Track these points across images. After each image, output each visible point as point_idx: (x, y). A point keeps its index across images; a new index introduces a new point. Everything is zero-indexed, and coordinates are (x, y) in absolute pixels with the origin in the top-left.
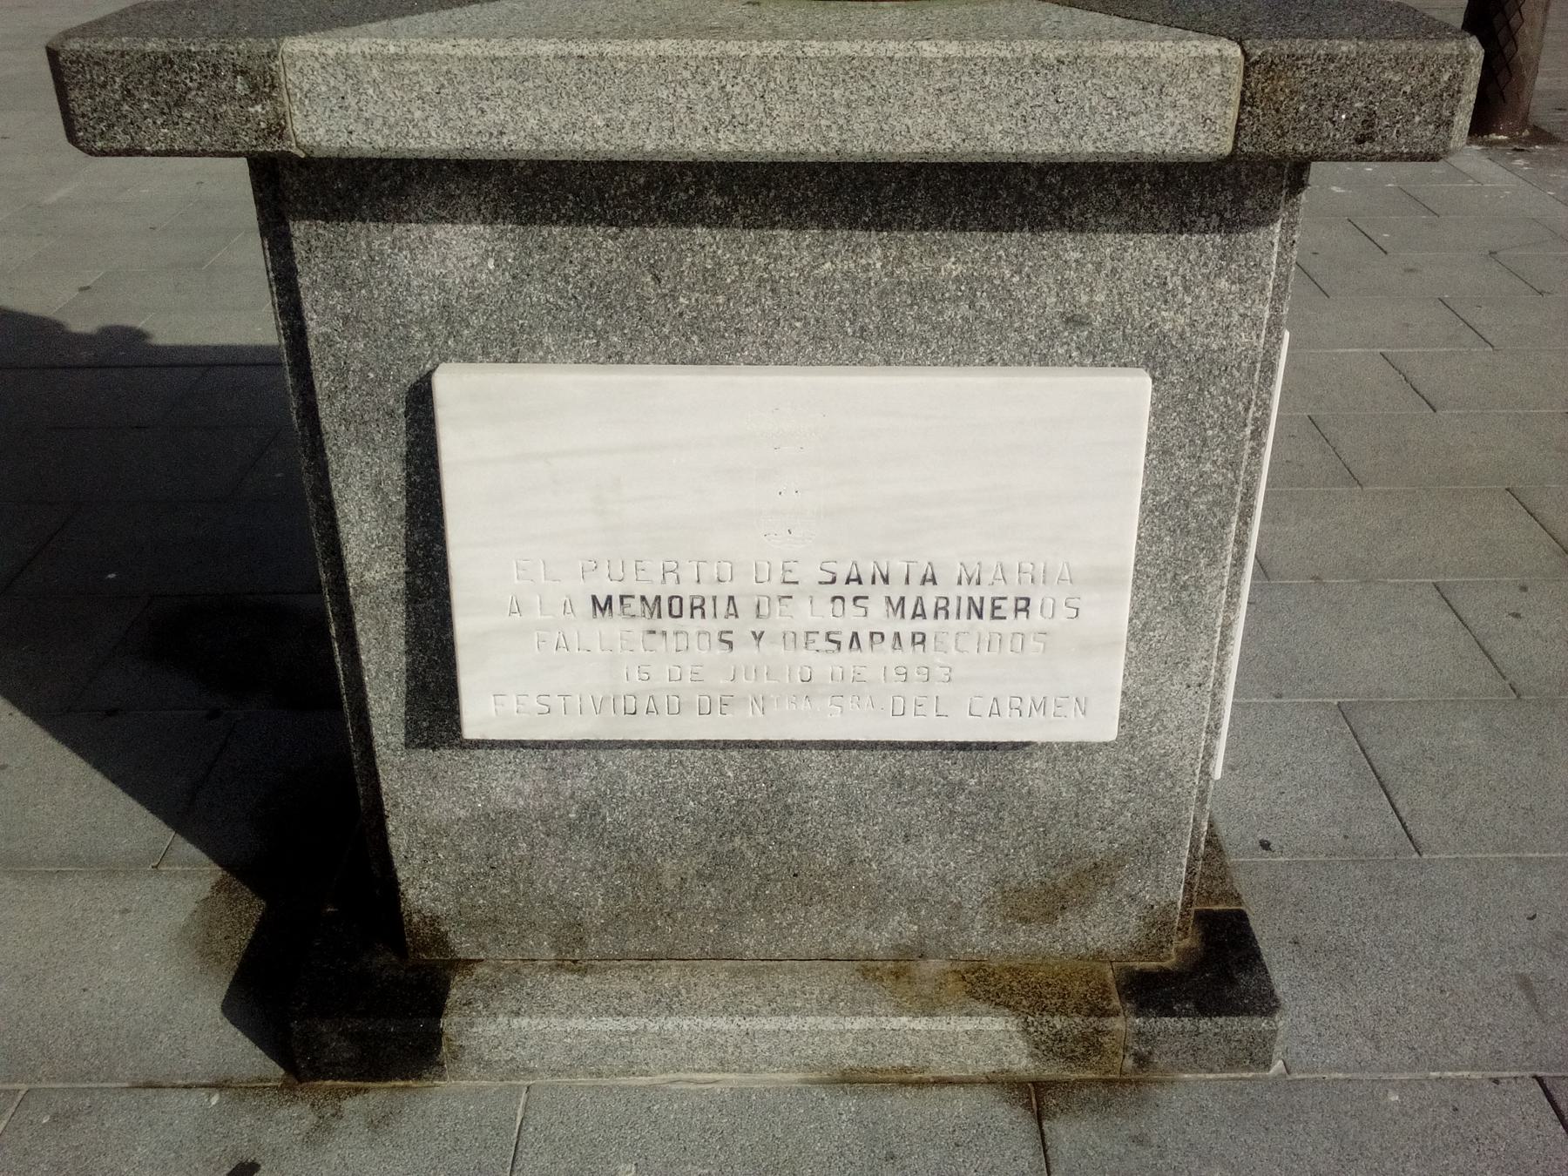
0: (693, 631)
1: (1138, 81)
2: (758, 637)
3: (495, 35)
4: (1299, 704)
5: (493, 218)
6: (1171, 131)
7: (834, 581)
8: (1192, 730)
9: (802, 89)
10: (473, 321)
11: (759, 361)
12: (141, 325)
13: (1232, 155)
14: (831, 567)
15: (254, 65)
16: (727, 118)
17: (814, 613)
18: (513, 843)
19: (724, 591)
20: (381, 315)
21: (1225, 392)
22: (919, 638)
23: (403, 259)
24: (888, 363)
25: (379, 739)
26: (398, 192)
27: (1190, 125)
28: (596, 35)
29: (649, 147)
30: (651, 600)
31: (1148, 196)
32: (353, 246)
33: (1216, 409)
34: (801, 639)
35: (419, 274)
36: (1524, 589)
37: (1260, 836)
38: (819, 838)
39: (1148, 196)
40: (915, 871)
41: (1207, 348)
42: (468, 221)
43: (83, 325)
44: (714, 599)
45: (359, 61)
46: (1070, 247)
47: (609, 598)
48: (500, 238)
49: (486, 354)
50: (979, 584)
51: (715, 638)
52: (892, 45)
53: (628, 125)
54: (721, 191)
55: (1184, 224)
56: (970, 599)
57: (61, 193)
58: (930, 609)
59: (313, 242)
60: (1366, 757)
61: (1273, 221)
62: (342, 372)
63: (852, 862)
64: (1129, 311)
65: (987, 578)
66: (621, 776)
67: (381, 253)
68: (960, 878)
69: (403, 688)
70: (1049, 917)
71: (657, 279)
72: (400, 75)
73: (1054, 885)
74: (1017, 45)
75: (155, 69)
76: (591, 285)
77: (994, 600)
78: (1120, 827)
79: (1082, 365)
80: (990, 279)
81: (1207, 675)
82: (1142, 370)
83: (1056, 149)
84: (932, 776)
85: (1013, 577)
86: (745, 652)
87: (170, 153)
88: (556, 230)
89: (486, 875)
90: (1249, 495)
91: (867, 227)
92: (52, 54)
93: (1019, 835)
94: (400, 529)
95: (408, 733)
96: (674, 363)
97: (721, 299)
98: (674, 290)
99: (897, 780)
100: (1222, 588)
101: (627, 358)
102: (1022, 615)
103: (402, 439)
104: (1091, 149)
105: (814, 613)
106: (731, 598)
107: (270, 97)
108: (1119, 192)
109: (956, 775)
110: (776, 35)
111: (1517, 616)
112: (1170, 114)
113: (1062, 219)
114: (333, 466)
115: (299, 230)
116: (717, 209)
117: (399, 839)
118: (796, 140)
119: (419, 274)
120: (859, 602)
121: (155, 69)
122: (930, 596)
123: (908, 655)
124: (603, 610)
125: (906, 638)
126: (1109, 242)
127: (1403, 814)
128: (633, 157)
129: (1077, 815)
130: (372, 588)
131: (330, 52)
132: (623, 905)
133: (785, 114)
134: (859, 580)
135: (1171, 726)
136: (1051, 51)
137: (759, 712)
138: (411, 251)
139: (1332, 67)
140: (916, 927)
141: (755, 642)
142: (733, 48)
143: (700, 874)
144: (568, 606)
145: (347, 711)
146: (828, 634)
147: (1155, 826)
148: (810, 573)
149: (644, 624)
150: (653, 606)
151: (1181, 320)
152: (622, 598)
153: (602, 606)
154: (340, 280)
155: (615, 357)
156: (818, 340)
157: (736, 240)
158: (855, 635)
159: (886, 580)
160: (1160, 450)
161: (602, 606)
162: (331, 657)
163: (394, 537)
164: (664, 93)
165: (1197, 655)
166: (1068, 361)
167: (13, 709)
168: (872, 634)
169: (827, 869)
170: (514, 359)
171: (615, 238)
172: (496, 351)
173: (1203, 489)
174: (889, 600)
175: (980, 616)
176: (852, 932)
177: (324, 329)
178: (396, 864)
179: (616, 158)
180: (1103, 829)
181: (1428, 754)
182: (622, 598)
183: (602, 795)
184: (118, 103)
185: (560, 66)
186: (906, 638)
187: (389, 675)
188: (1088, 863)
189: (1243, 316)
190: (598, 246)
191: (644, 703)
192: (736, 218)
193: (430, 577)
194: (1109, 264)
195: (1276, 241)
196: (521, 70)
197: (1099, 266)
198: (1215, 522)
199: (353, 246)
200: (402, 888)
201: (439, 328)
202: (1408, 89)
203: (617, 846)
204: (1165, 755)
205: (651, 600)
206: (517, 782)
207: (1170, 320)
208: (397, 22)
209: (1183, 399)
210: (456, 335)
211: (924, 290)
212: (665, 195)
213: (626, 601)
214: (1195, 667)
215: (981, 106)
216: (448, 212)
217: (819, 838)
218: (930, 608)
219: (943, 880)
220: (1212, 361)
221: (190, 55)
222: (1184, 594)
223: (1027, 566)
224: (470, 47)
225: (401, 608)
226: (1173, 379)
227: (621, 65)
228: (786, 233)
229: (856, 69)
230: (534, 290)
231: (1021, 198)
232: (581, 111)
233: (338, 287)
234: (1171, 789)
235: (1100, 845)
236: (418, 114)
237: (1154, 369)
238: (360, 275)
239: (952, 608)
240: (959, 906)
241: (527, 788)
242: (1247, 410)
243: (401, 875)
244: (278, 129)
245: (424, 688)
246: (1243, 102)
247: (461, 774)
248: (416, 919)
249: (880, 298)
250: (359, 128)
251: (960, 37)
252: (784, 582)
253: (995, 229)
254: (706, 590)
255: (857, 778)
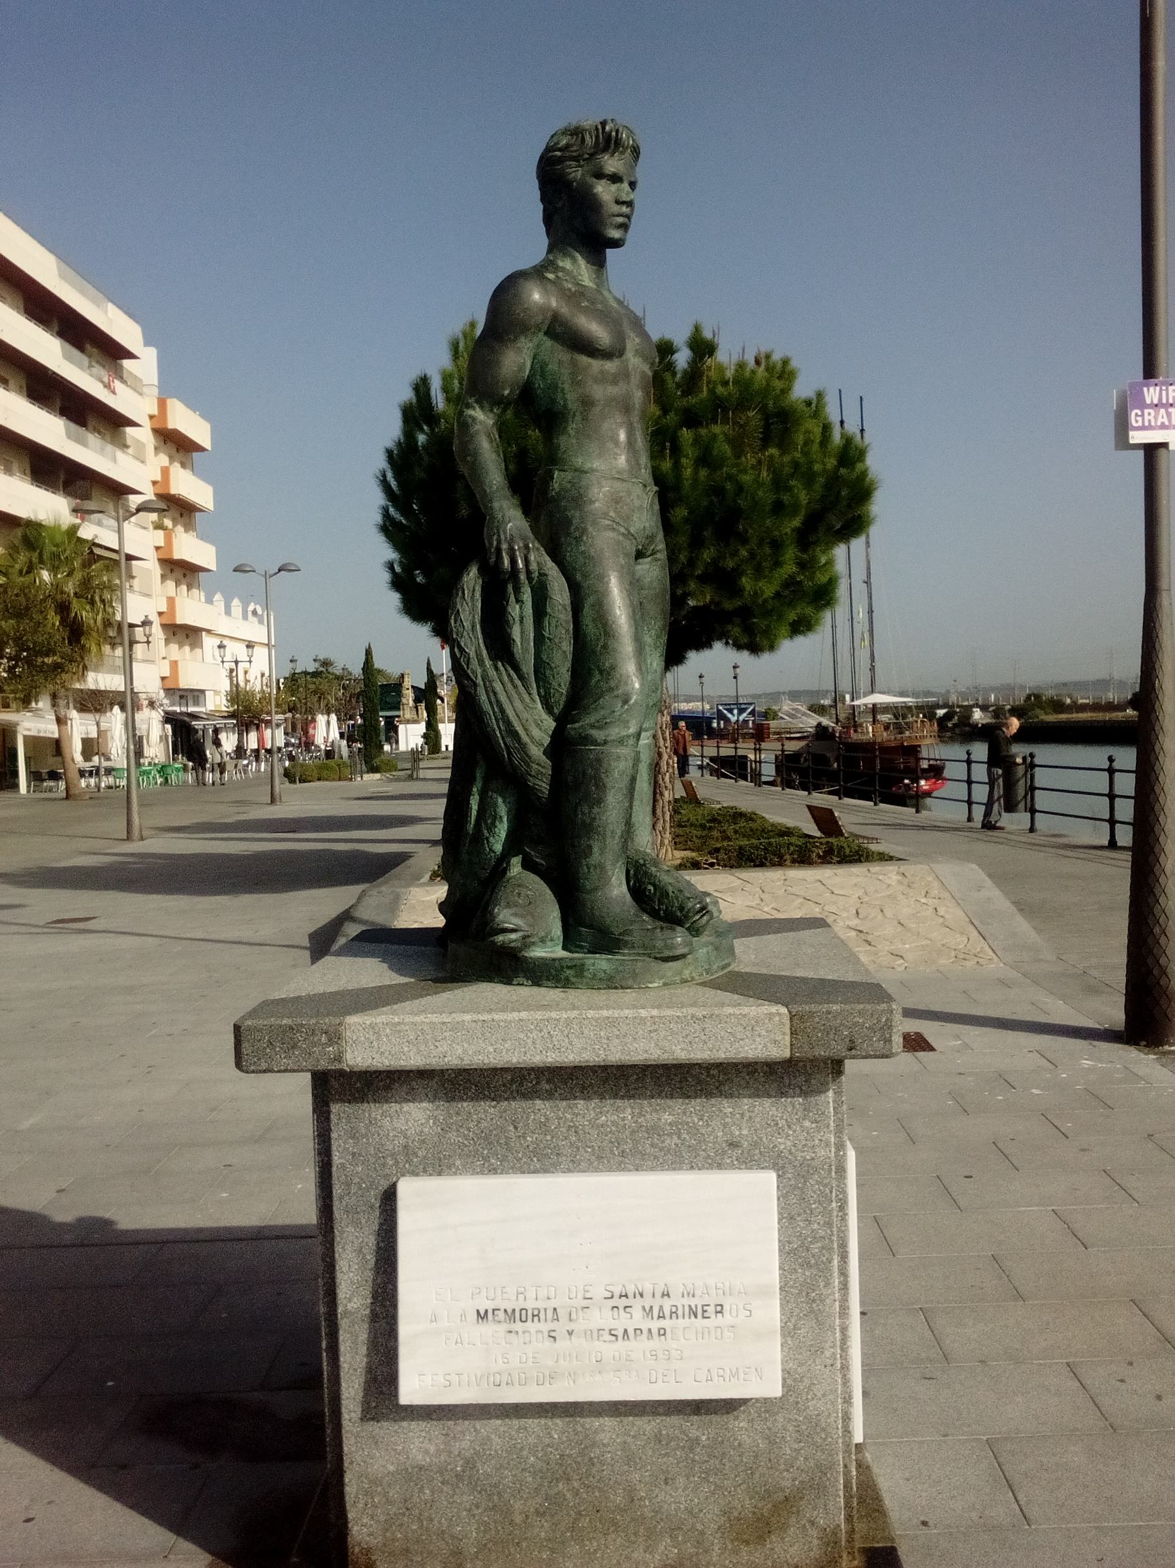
0: (533, 1331)
1: (741, 1025)
2: (570, 1333)
3: (444, 1012)
4: (959, 1440)
5: (435, 1098)
6: (760, 1047)
7: (612, 1297)
8: (831, 1397)
9: (586, 1032)
10: (420, 1153)
11: (569, 1171)
12: (107, 1216)
13: (791, 1058)
14: (611, 1288)
15: (332, 1029)
16: (551, 1046)
17: (601, 1318)
18: (421, 1490)
19: (553, 1304)
20: (372, 1152)
21: (818, 1183)
22: (662, 1332)
23: (386, 1122)
24: (637, 1170)
25: (345, 1416)
26: (388, 1088)
27: (769, 1044)
28: (490, 1011)
29: (515, 1060)
30: (510, 1311)
31: (763, 1079)
32: (362, 1116)
33: (814, 1192)
34: (595, 1334)
35: (394, 1129)
36: (1131, 1364)
37: (922, 1519)
38: (611, 1482)
39: (763, 1079)
40: (673, 1506)
41: (805, 1159)
42: (421, 1101)
43: (63, 1215)
44: (545, 1310)
45: (380, 1025)
46: (726, 1106)
47: (486, 1311)
48: (437, 1109)
49: (425, 1171)
50: (693, 1296)
51: (546, 1334)
52: (627, 1011)
53: (504, 1051)
54: (548, 1081)
55: (782, 1093)
56: (690, 1306)
57: (32, 1121)
58: (667, 1313)
59: (342, 1115)
60: (1001, 1470)
61: (828, 1090)
62: (348, 1185)
63: (633, 1500)
64: (761, 1139)
65: (698, 1293)
66: (489, 1439)
67: (376, 1119)
68: (701, 1511)
69: (362, 1380)
70: (761, 1539)
71: (516, 1128)
72: (400, 1031)
73: (762, 1515)
74: (684, 1010)
75: (284, 1032)
76: (482, 1132)
77: (703, 1306)
78: (797, 1469)
79: (740, 1169)
80: (687, 1123)
81: (835, 1359)
82: (772, 1171)
83: (707, 1057)
84: (679, 1435)
85: (713, 1292)
86: (563, 1344)
87: (285, 1071)
88: (465, 1104)
89: (404, 1514)
90: (843, 1246)
91: (622, 1098)
92: (237, 1028)
93: (736, 1476)
94: (369, 1274)
95: (363, 1411)
96: (524, 1173)
97: (549, 1138)
98: (525, 1133)
99: (658, 1438)
100: (835, 1301)
101: (499, 1171)
102: (720, 1315)
103: (377, 1222)
104: (724, 1056)
105: (601, 1318)
106: (555, 1309)
107: (337, 1043)
108: (747, 1077)
109: (694, 1433)
110: (574, 1008)
111: (1122, 1381)
112: (758, 1039)
113: (721, 1092)
114: (338, 1239)
115: (335, 1108)
116: (547, 1091)
117: (351, 1489)
118: (584, 1055)
119: (394, 1129)
120: (627, 1310)
121: (284, 1032)
122: (667, 1305)
123: (656, 1343)
124: (482, 1318)
125: (655, 1332)
126: (746, 1102)
127: (1021, 1503)
128: (507, 1066)
129: (770, 1460)
130: (351, 1313)
131: (368, 1022)
132: (488, 1537)
133: (578, 1043)
134: (626, 1296)
135: (819, 1395)
136: (700, 1012)
137: (572, 1383)
138: (391, 1118)
139: (830, 1016)
140: (676, 1551)
141: (568, 1336)
142: (554, 1015)
143: (537, 1513)
144: (463, 1316)
145: (326, 1400)
146: (610, 1330)
147: (819, 1466)
148: (599, 1292)
149: (505, 1327)
150: (511, 1315)
151: (789, 1143)
152: (494, 1310)
153: (482, 1316)
154: (353, 1135)
155: (493, 1171)
156: (599, 1158)
157: (557, 1106)
158: (626, 1331)
159: (641, 1295)
160: (787, 1217)
161: (482, 1316)
162: (321, 1364)
163: (366, 1281)
164: (522, 1036)
165: (828, 1345)
166: (732, 1167)
167: (53, 1467)
168: (635, 1330)
169: (617, 1507)
170: (440, 1174)
171: (494, 1107)
172: (430, 1170)
173: (815, 1239)
174: (644, 1308)
175: (696, 1317)
176: (635, 1555)
177: (341, 1161)
178: (348, 1508)
179: (498, 1066)
180: (788, 1471)
181: (1044, 1467)
182: (494, 1310)
183: (477, 1453)
184: (265, 1048)
185: (474, 1025)
186: (655, 1332)
187: (355, 1370)
188: (780, 1496)
189: (821, 1140)
190: (485, 1111)
191: (505, 1378)
192: (557, 1095)
193: (385, 1306)
194: (747, 1115)
195: (831, 1100)
196: (456, 1027)
197: (742, 1115)
198: (825, 1259)
199: (362, 1116)
200: (350, 1525)
201: (401, 1158)
202: (867, 1025)
203: (486, 1491)
204: (818, 1415)
205: (510, 1311)
206: (426, 1445)
207: (783, 1144)
208: (395, 1007)
209: (796, 1187)
210: (409, 1161)
211: (654, 1130)
212: (521, 1084)
213: (496, 1312)
214: (828, 1354)
215: (670, 1038)
216: (411, 1097)
217: (611, 1482)
218: (667, 1313)
219: (691, 1512)
220: (809, 1166)
221: (302, 1025)
222: (814, 1305)
223: (720, 1285)
224: (434, 1018)
225: (366, 1326)
226: (790, 1176)
227: (502, 1024)
228: (582, 1102)
229: (612, 1022)
230: (453, 1136)
231: (699, 1082)
232: (483, 1045)
233: (352, 1138)
234: (825, 1439)
235: (787, 1482)
236: (406, 1049)
237: (778, 1170)
238: (363, 1131)
239: (680, 1312)
240: (702, 1533)
241: (432, 1449)
242: (831, 1192)
243: (350, 1516)
244: (339, 1058)
245: (375, 1379)
246: (792, 1033)
247: (393, 1439)
248: (357, 1550)
249: (631, 1135)
250: (377, 1056)
251: (659, 1007)
252: (585, 1298)
253: (689, 1097)
254: (541, 1305)
255: (634, 1437)
